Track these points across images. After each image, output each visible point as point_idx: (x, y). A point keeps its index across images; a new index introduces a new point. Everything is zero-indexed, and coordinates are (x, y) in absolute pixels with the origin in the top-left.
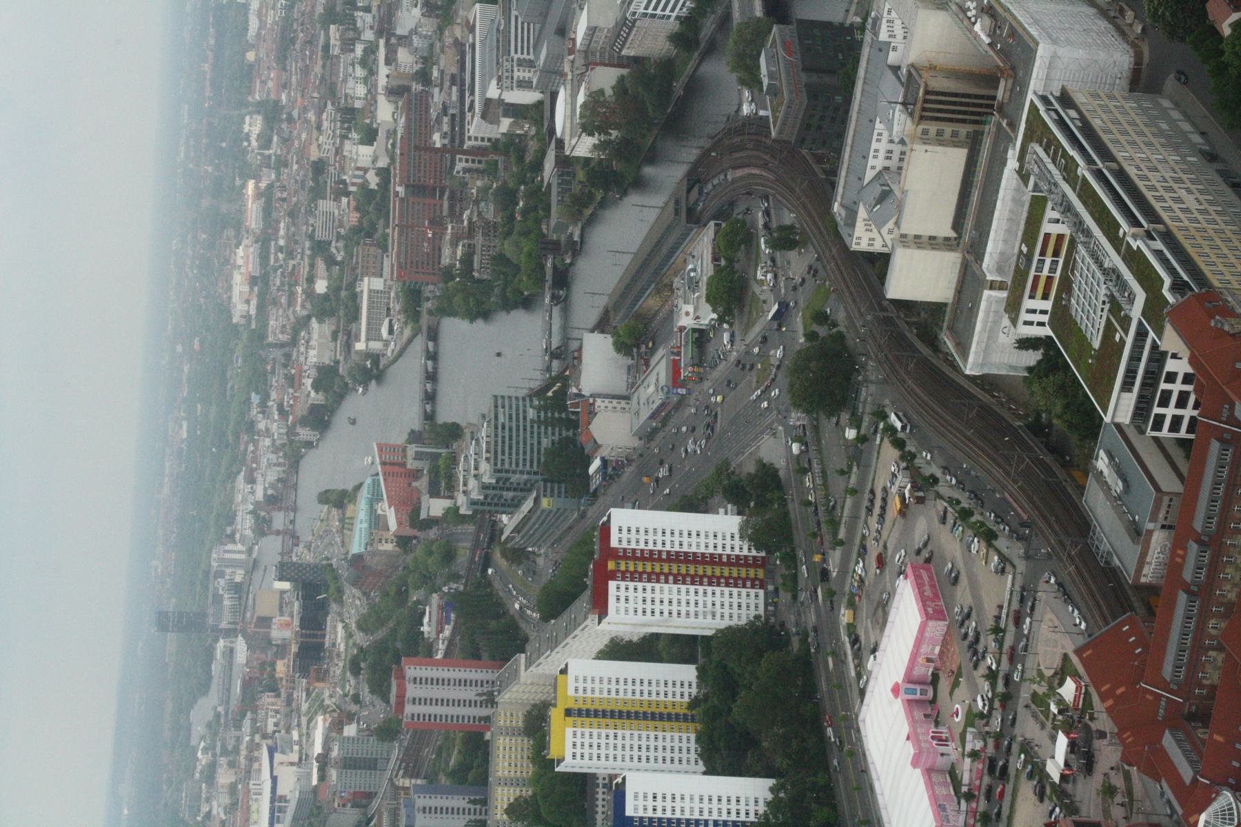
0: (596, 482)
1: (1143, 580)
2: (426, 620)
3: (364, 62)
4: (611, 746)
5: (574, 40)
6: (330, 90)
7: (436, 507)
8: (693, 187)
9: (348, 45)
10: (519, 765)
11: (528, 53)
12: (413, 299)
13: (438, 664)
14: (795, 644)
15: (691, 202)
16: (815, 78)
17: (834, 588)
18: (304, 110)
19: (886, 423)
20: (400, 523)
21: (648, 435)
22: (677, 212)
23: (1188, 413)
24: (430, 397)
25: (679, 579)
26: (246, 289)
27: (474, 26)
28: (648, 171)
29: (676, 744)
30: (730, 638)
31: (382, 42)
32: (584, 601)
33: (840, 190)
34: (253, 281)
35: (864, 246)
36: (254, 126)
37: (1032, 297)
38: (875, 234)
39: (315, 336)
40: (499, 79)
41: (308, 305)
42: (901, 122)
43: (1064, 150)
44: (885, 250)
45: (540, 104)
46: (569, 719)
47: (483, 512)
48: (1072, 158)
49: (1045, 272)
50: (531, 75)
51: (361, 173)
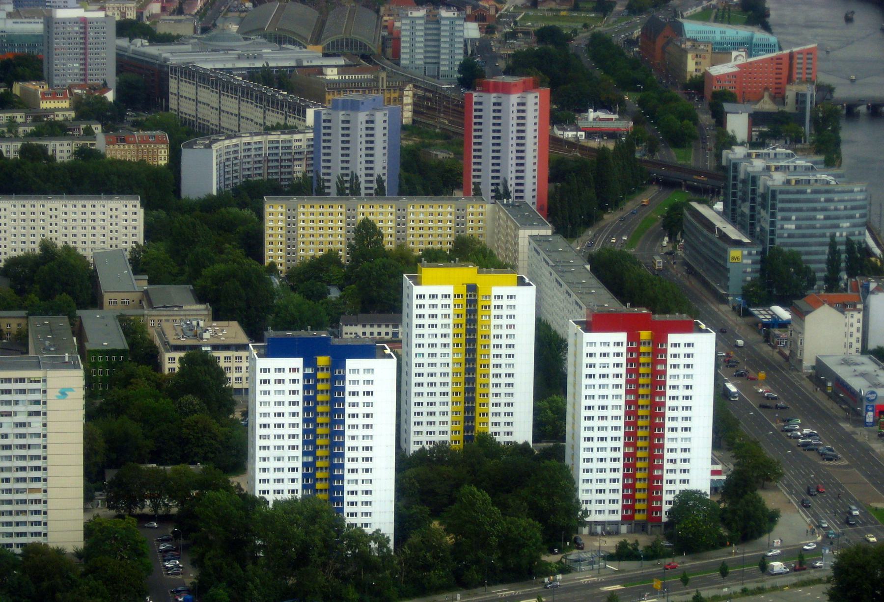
0: (762, 315)
2: (601, 114)
10: (431, 232)
14: (552, 559)
20: (720, 78)
25: (631, 414)
29: (437, 418)
32: (610, 303)
46: (463, 290)
47: (726, 179)
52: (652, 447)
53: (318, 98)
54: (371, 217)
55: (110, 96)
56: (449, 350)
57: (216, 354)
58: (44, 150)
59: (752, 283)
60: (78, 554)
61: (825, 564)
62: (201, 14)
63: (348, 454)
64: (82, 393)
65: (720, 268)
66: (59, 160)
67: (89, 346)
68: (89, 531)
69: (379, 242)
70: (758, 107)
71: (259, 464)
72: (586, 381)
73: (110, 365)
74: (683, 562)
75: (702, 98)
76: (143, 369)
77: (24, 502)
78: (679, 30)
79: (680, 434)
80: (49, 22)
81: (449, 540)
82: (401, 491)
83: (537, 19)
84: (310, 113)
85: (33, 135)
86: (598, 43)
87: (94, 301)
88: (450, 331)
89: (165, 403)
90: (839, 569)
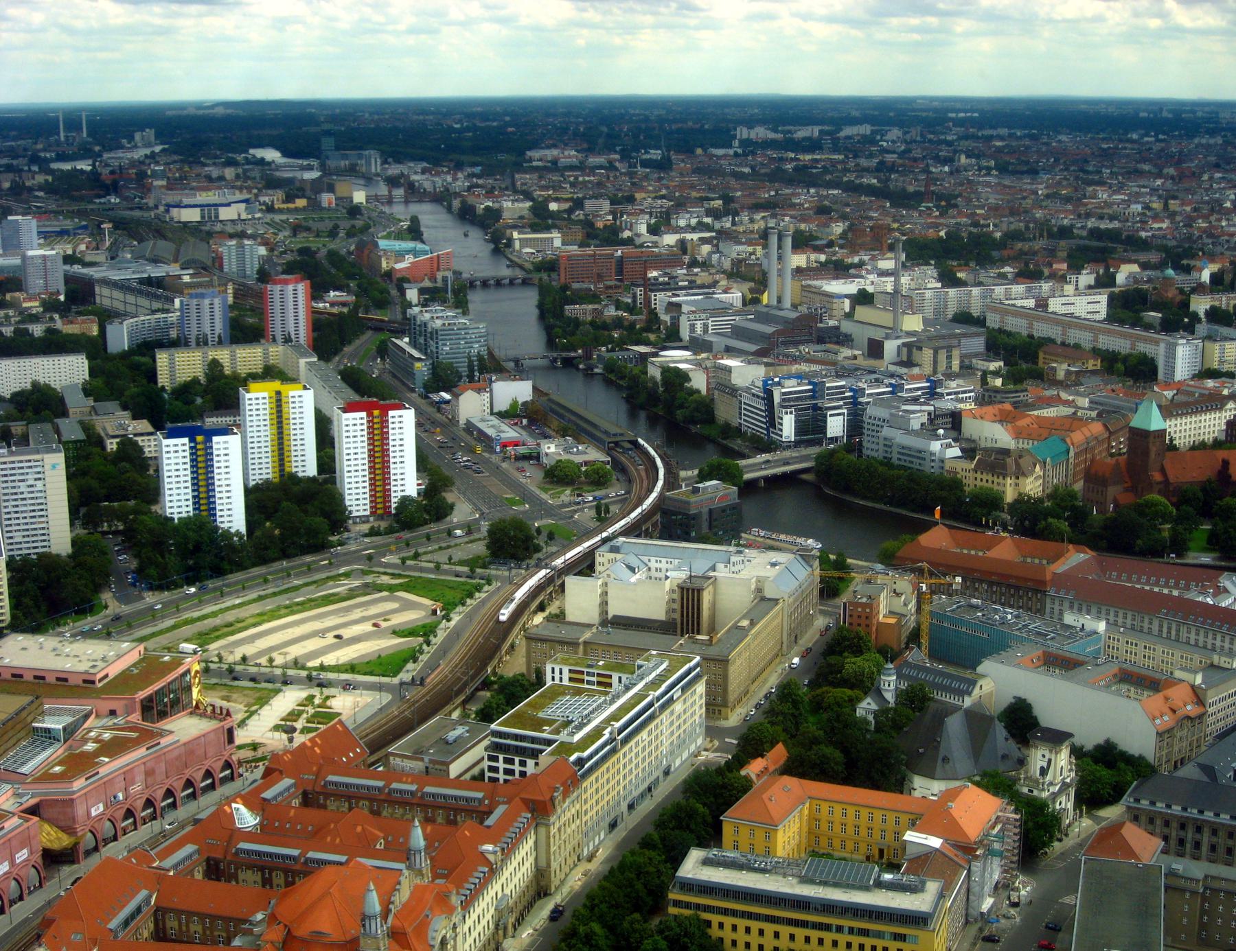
0: (435, 397)
2: (337, 293)
3: (700, 223)
7: (412, 294)
9: (709, 212)
12: (550, 266)
16: (705, 516)
17: (375, 560)
18: (667, 188)
21: (470, 428)
23: (501, 776)
25: (372, 456)
28: (643, 415)
29: (264, 466)
32: (355, 397)
34: (555, 162)
37: (570, 671)
39: (521, 205)
42: (679, 575)
45: (681, 340)
46: (273, 394)
52: (384, 473)
53: (180, 293)
55: (62, 298)
58: (27, 330)
59: (428, 381)
60: (69, 556)
61: (485, 526)
62: (109, 249)
63: (217, 489)
64: (63, 466)
65: (411, 374)
67: (64, 439)
68: (74, 543)
69: (221, 371)
70: (422, 285)
71: (168, 498)
72: (345, 440)
73: (76, 449)
74: (406, 535)
76: (96, 450)
78: (376, 245)
80: (24, 258)
81: (277, 532)
83: (295, 243)
84: (177, 302)
85: (19, 322)
86: (332, 254)
87: (64, 413)
88: (267, 417)
89: (111, 468)
90: (491, 533)
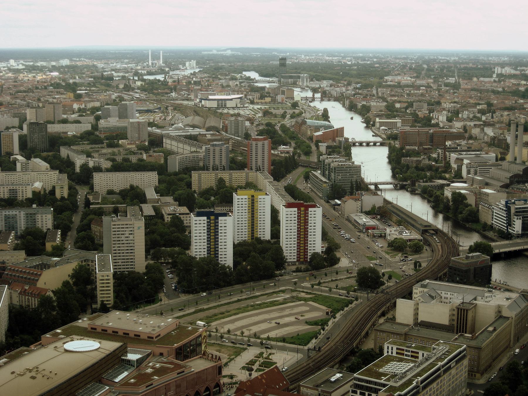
0: (333, 202)
1: (302, 388)
2: (285, 147)
3: (474, 117)
4: (242, 211)
5: (484, 188)
6: (465, 107)
8: (435, 231)
11: (479, 173)
13: (270, 152)
14: (278, 272)
15: (429, 231)
19: (354, 300)
20: (317, 136)
22: (426, 226)
24: (361, 144)
25: (299, 231)
26: (396, 81)
27: (488, 154)
28: (441, 216)
30: (279, 250)
31: (482, 123)
32: (292, 201)
33: (433, 282)
34: (399, 83)
35: (414, 291)
36: (452, 80)
37: (397, 349)
38: (419, 294)
39: (381, 104)
40: (470, 163)
41: (391, 102)
43: (447, 357)
44: (413, 298)
45: (462, 178)
46: (250, 197)
48: (445, 360)
49: (406, 353)
50: (472, 174)
51: (437, 117)
54: (222, 177)
55: (147, 144)
56: (247, 214)
57: (180, 216)
58: (129, 159)
66: (133, 162)
67: (144, 214)
69: (224, 184)
74: (315, 272)
75: (312, 142)
77: (128, 259)
79: (312, 236)
82: (235, 254)
84: (204, 148)
